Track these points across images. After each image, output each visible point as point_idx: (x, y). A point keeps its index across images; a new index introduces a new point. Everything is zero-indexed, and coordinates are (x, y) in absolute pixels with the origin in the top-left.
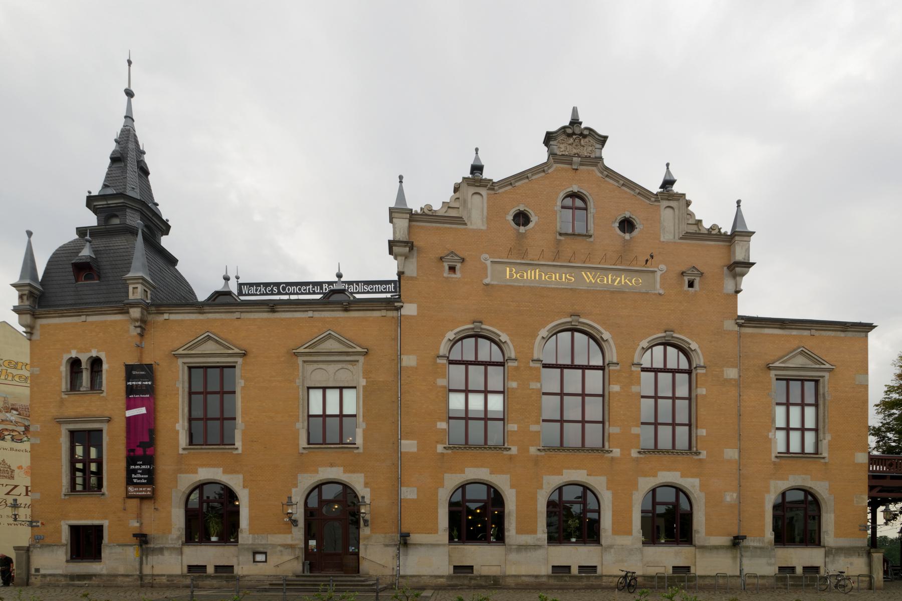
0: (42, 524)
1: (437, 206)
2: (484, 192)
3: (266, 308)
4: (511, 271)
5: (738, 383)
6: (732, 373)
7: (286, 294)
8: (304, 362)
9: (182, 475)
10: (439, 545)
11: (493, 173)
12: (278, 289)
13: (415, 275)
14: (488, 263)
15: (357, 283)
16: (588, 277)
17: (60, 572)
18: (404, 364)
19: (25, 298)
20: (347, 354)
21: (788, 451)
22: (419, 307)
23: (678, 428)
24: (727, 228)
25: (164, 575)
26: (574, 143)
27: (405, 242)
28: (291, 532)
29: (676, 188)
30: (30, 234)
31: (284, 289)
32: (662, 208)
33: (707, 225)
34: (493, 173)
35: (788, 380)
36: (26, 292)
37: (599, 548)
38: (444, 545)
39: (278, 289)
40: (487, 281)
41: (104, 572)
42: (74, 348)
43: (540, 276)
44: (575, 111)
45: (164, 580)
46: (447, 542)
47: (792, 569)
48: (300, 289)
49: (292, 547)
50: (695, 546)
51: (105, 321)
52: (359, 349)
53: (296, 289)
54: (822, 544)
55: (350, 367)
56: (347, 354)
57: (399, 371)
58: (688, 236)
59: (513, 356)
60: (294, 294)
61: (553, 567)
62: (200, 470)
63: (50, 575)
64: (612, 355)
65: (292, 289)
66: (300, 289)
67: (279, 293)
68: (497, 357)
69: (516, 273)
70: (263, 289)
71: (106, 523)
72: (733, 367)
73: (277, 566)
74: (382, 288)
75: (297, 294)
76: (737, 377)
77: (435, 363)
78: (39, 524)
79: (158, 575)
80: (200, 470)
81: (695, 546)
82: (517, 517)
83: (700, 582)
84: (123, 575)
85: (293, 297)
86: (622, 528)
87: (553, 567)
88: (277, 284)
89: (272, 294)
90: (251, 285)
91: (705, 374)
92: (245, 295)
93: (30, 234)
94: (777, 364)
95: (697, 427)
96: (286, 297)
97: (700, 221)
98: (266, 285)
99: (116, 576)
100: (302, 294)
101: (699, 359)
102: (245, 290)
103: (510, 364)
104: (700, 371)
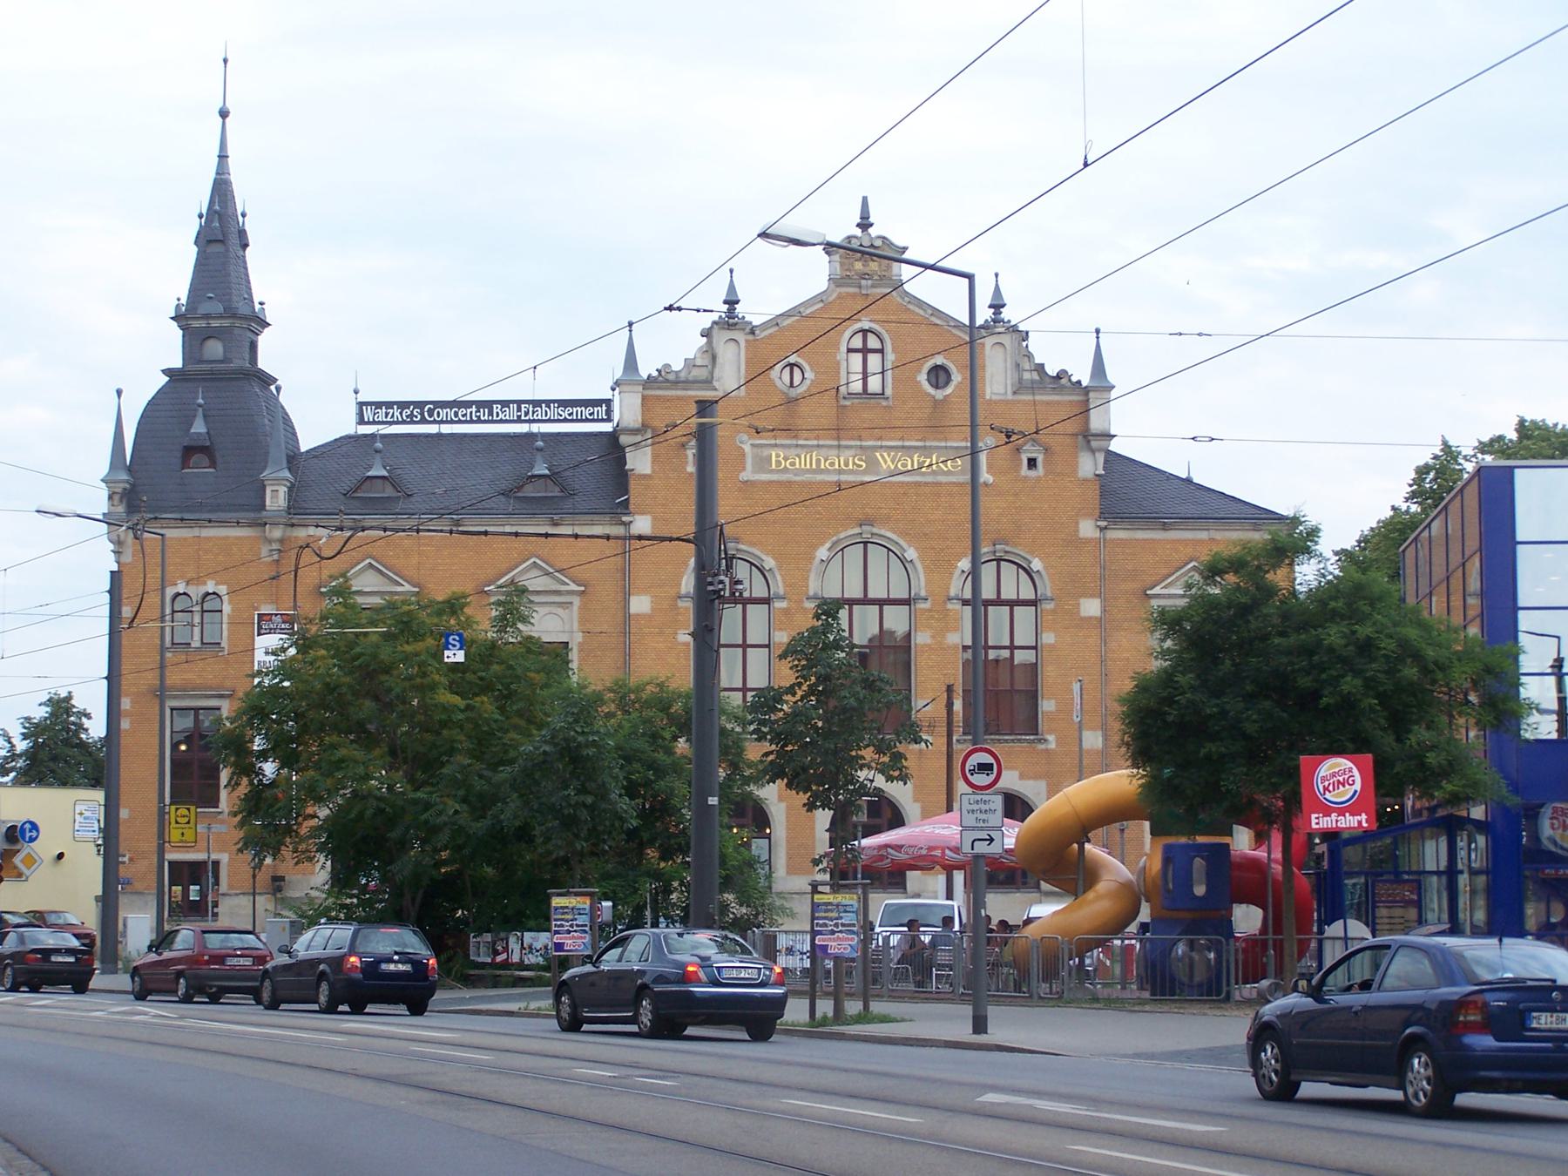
0: (131, 859)
1: (677, 366)
2: (741, 337)
4: (778, 456)
5: (1101, 624)
6: (1091, 607)
7: (435, 422)
11: (755, 310)
12: (422, 414)
13: (648, 471)
14: (747, 448)
15: (548, 403)
16: (886, 462)
18: (633, 610)
19: (117, 498)
22: (654, 519)
24: (1082, 374)
26: (866, 259)
29: (1006, 314)
30: (119, 393)
31: (431, 413)
32: (988, 347)
33: (1052, 370)
34: (755, 310)
39: (422, 414)
40: (744, 476)
43: (818, 461)
48: (456, 414)
51: (227, 538)
52: (573, 587)
53: (450, 413)
55: (560, 611)
57: (627, 617)
58: (1033, 388)
59: (781, 592)
60: (447, 422)
64: (921, 586)
65: (444, 413)
66: (456, 414)
67: (423, 421)
68: (1027, 593)
69: (786, 459)
70: (397, 414)
72: (1092, 596)
74: (586, 412)
75: (452, 422)
76: (1098, 614)
77: (675, 607)
78: (126, 859)
82: (789, 849)
85: (446, 429)
88: (420, 405)
89: (413, 422)
90: (378, 405)
91: (1054, 611)
92: (369, 423)
93: (119, 393)
94: (1157, 590)
96: (432, 429)
97: (1042, 366)
98: (403, 405)
100: (460, 422)
101: (1046, 588)
102: (368, 414)
103: (778, 604)
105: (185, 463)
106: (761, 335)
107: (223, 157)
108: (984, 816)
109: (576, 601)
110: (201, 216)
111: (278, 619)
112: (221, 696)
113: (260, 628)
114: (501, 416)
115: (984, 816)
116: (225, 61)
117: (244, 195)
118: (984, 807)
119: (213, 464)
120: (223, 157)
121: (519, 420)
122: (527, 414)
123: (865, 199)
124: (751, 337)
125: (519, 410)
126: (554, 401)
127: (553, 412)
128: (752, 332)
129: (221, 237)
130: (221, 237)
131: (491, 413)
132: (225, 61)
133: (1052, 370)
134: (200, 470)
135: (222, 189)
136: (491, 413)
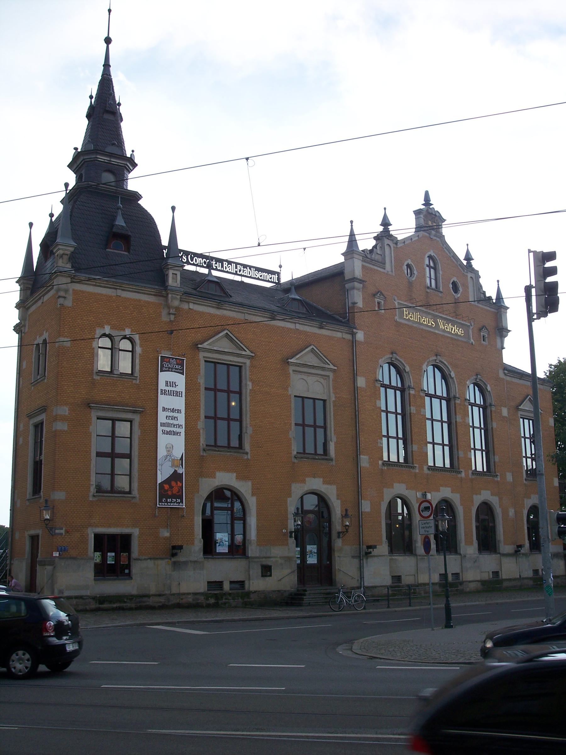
0: (67, 532)
3: (268, 315)
7: (194, 264)
8: (294, 371)
9: (204, 479)
10: (384, 556)
15: (250, 267)
17: (88, 593)
20: (323, 369)
21: (304, 452)
22: (365, 334)
23: (226, 416)
25: (188, 594)
27: (361, 280)
28: (287, 544)
35: (228, 365)
36: (69, 253)
37: (494, 556)
38: (387, 556)
41: (134, 592)
42: (108, 323)
44: (427, 194)
45: (190, 599)
46: (387, 553)
47: (220, 584)
49: (288, 559)
50: (499, 553)
51: (139, 301)
52: (332, 366)
54: (498, 551)
55: (322, 380)
56: (323, 369)
57: (355, 389)
61: (208, 582)
62: (218, 474)
63: (77, 597)
71: (135, 532)
73: (280, 580)
79: (184, 594)
80: (218, 474)
81: (499, 553)
83: (505, 584)
84: (155, 595)
86: (469, 542)
87: (208, 582)
95: (412, 444)
96: (238, 278)
99: (148, 596)
104: (412, 392)
105: (107, 245)
106: (400, 245)
107: (107, 65)
108: (428, 530)
109: (331, 375)
110: (91, 97)
111: (174, 362)
112: (134, 412)
113: (162, 366)
114: (228, 269)
115: (428, 530)
116: (110, 11)
117: (121, 92)
118: (427, 525)
119: (128, 250)
120: (107, 65)
121: (236, 274)
122: (240, 271)
123: (427, 194)
124: (395, 245)
125: (236, 268)
126: (253, 267)
127: (253, 273)
128: (396, 244)
129: (104, 113)
130: (104, 113)
131: (222, 266)
132: (110, 11)
133: (487, 295)
134: (117, 252)
135: (106, 84)
136: (222, 266)
